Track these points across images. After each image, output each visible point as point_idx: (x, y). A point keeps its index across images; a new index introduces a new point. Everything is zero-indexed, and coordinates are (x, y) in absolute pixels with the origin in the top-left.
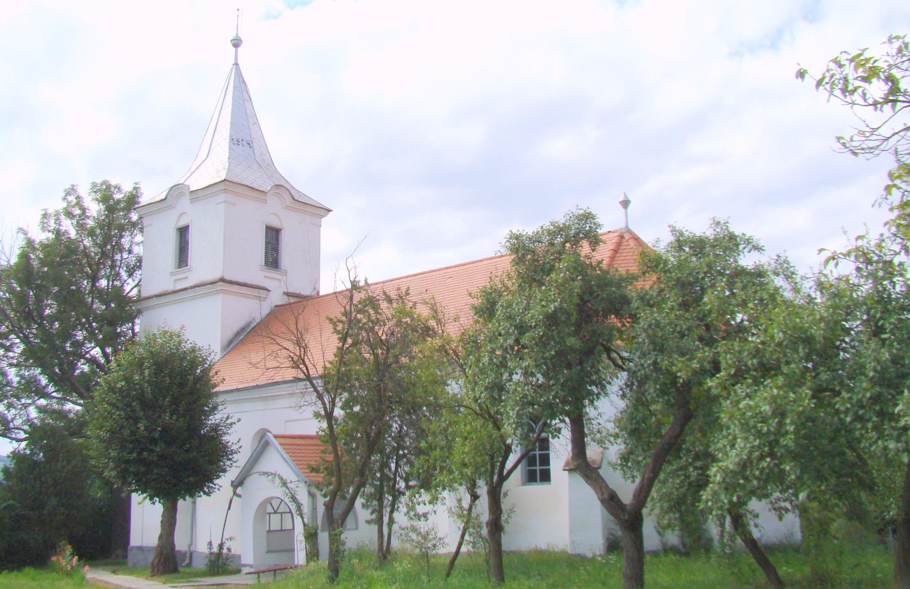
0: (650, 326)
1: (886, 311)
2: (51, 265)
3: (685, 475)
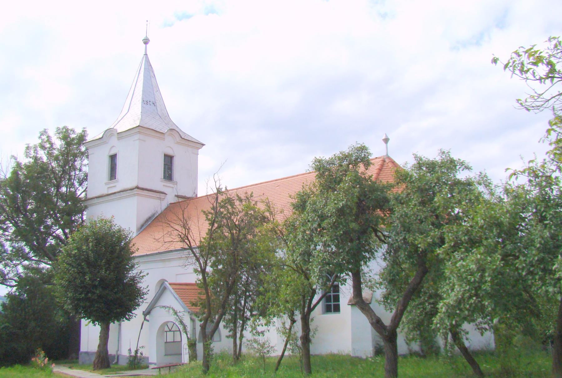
0: (401, 216)
2: (31, 178)
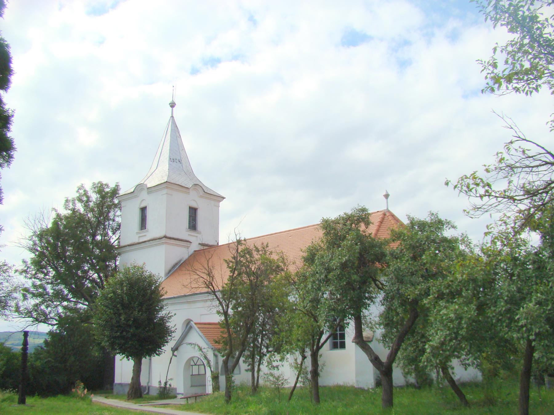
0: (395, 270)
1: (515, 265)
2: (70, 228)
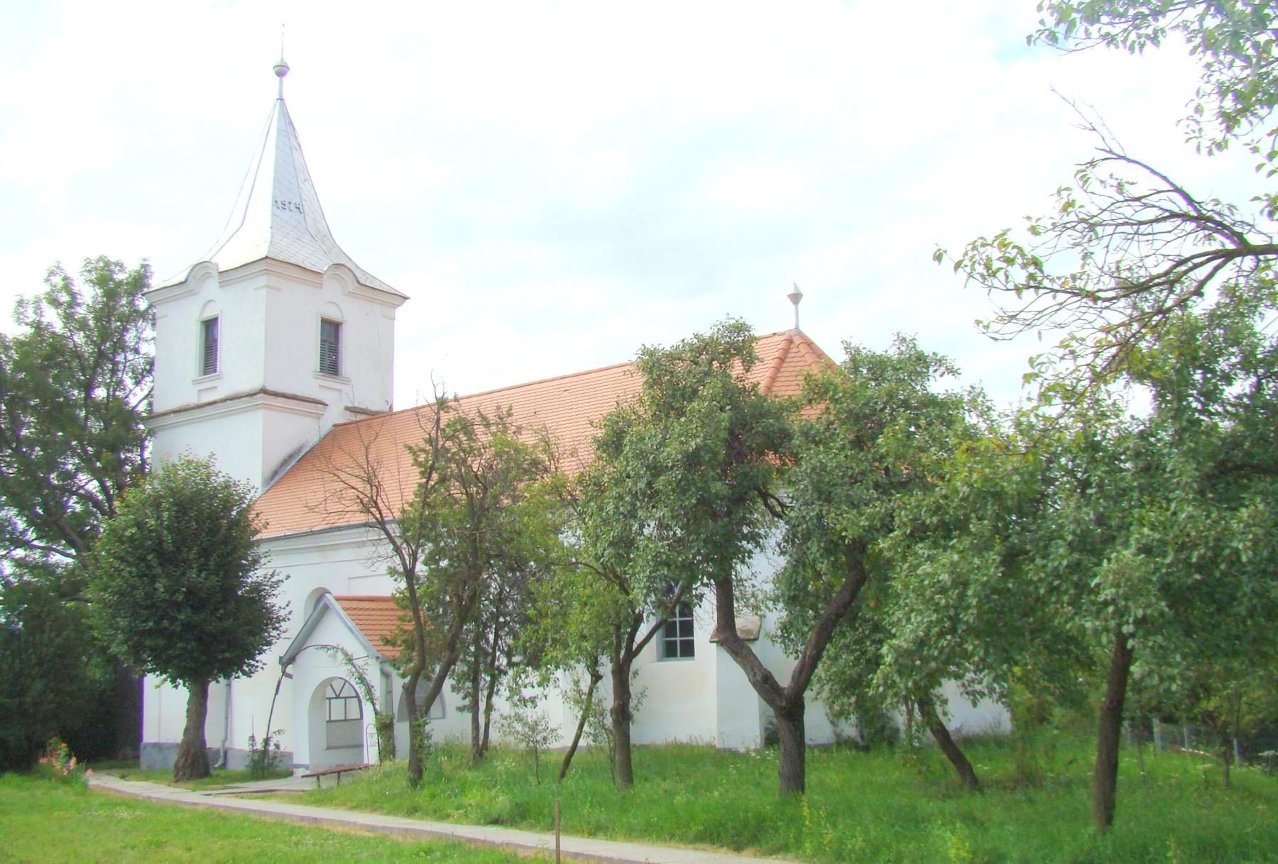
0: (813, 469)
3: (859, 650)
